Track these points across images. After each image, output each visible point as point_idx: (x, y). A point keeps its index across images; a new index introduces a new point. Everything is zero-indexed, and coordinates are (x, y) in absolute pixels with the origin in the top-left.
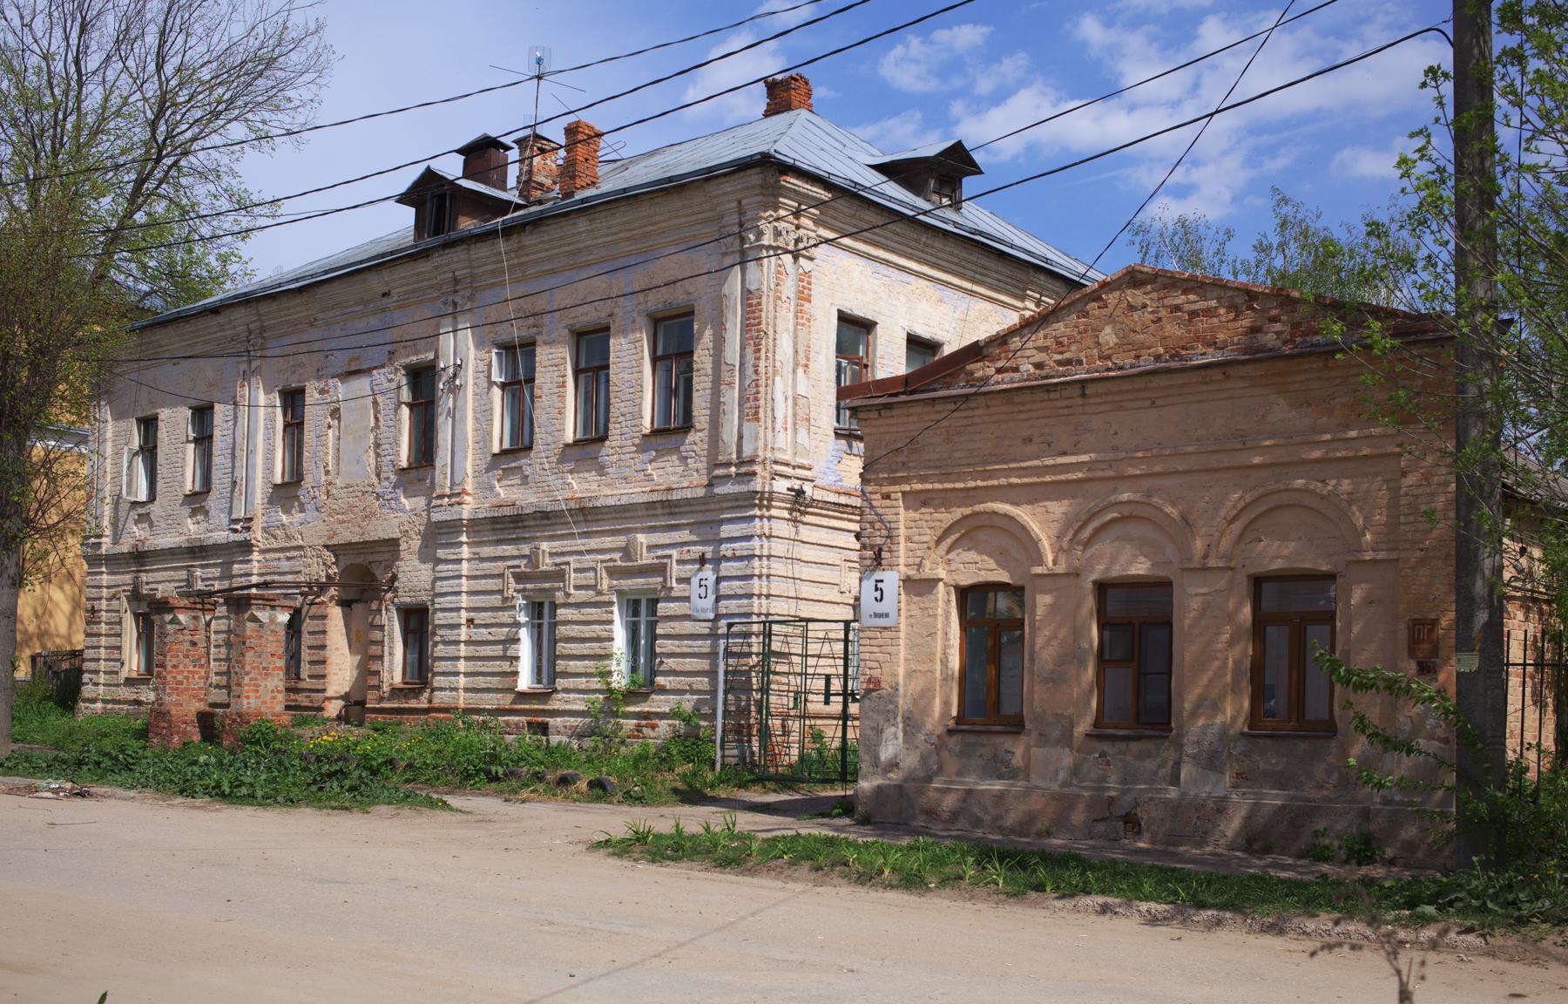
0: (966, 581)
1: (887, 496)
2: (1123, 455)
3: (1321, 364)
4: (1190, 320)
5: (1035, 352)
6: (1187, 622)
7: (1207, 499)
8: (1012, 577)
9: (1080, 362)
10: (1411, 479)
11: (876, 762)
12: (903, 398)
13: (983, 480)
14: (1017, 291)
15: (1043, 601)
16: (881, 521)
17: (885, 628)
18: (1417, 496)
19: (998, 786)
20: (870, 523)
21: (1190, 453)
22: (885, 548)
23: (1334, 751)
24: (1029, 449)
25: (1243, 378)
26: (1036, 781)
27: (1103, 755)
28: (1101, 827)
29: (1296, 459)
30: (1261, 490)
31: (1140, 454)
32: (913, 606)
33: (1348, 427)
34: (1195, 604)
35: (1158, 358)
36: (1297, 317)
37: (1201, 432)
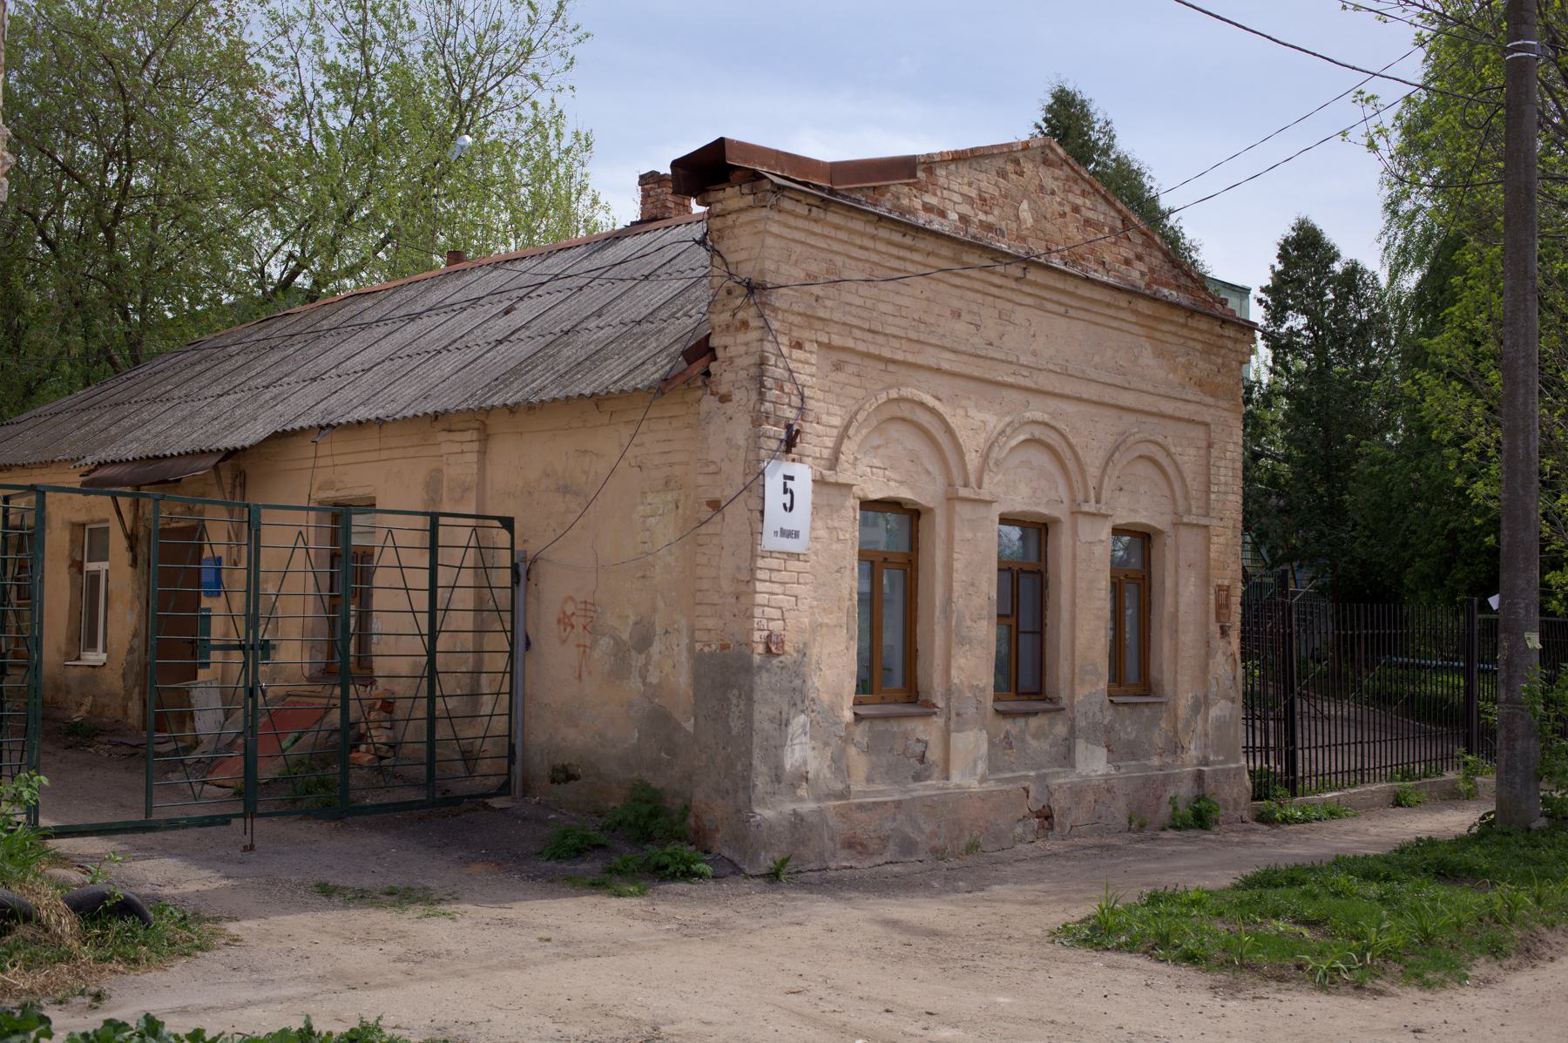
1: (799, 346)
11: (777, 776)
25: (1135, 312)
32: (819, 524)
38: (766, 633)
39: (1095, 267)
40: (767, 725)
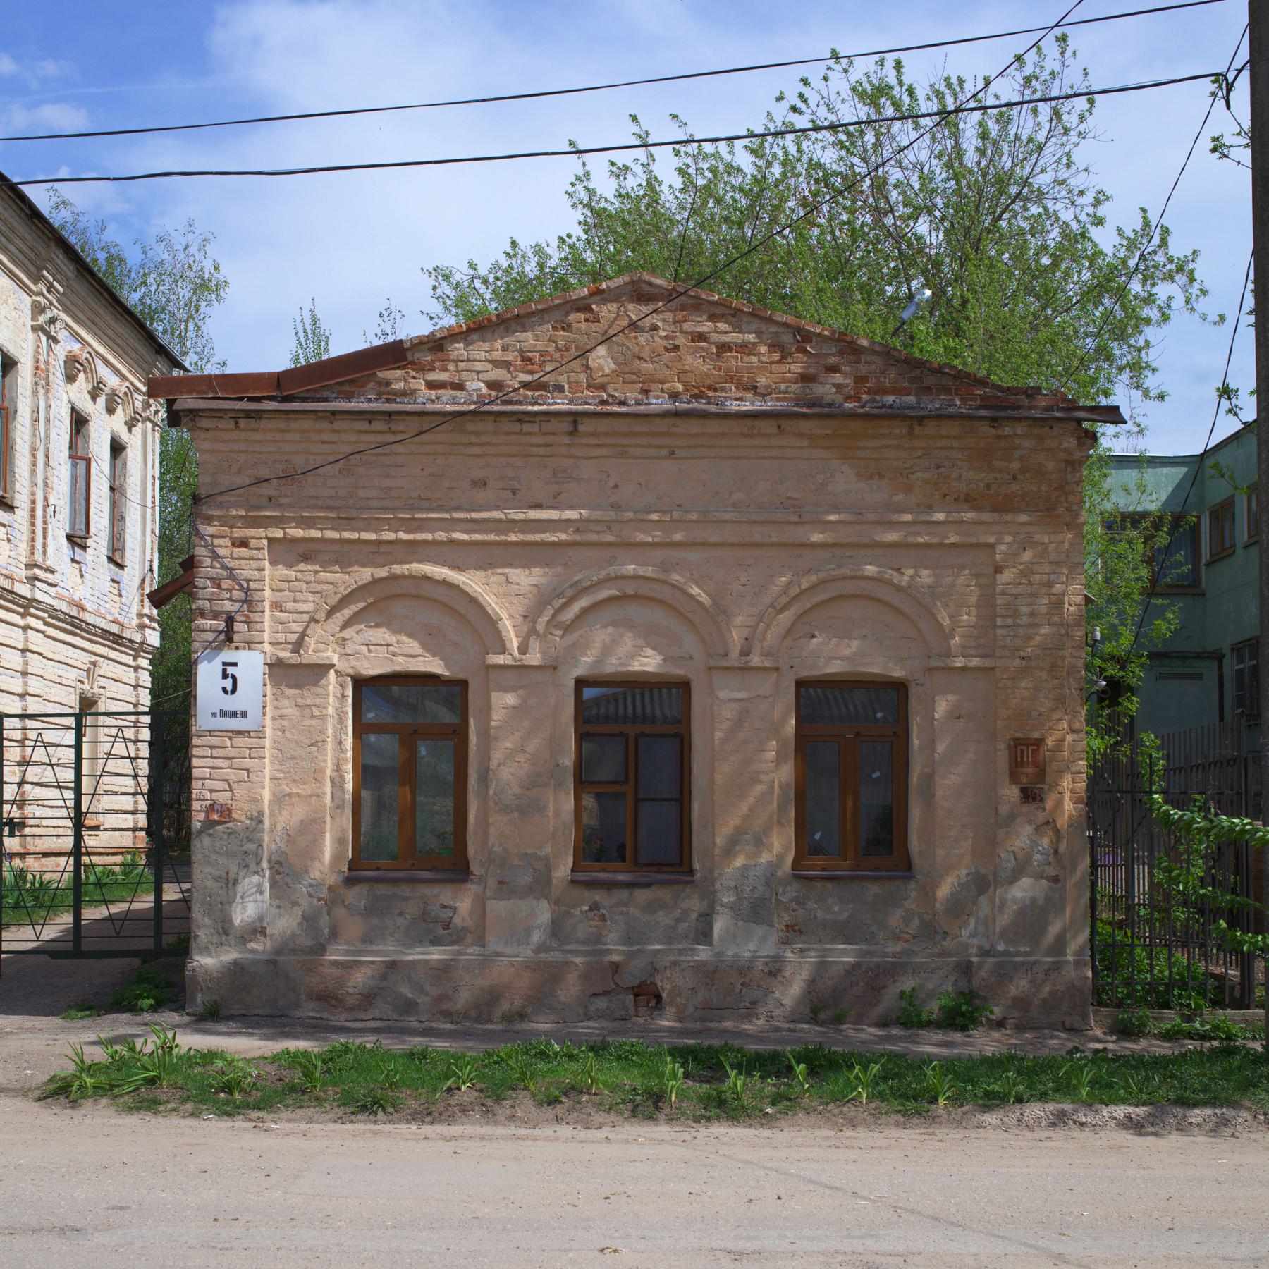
0: (371, 668)
1: (244, 543)
2: (630, 515)
3: (904, 431)
4: (718, 354)
5: (489, 366)
6: (718, 735)
7: (743, 580)
8: (448, 667)
9: (560, 388)
10: (1006, 576)
11: (225, 927)
12: (273, 405)
13: (407, 531)
14: (32, 269)
15: (503, 701)
16: (232, 577)
17: (239, 733)
18: (1016, 596)
19: (436, 954)
20: (211, 579)
21: (725, 522)
22: (239, 617)
23: (914, 894)
24: (482, 495)
25: (802, 435)
26: (494, 944)
27: (594, 907)
28: (602, 1003)
29: (866, 541)
30: (822, 575)
31: (655, 517)
33: (930, 508)
34: (728, 713)
35: (674, 396)
36: (863, 369)
37: (738, 496)
38: (208, 803)
39: (739, 395)
40: (210, 884)
